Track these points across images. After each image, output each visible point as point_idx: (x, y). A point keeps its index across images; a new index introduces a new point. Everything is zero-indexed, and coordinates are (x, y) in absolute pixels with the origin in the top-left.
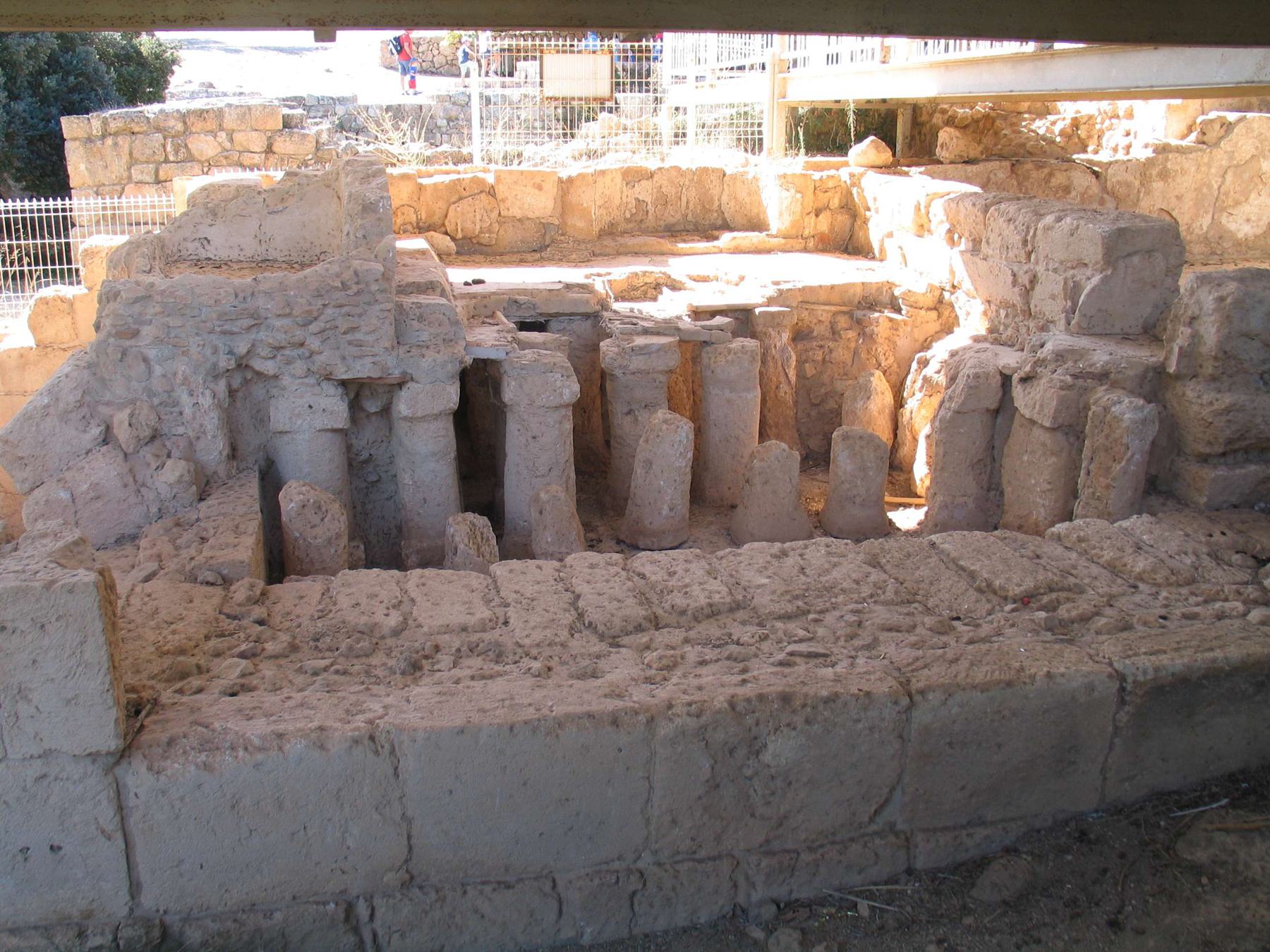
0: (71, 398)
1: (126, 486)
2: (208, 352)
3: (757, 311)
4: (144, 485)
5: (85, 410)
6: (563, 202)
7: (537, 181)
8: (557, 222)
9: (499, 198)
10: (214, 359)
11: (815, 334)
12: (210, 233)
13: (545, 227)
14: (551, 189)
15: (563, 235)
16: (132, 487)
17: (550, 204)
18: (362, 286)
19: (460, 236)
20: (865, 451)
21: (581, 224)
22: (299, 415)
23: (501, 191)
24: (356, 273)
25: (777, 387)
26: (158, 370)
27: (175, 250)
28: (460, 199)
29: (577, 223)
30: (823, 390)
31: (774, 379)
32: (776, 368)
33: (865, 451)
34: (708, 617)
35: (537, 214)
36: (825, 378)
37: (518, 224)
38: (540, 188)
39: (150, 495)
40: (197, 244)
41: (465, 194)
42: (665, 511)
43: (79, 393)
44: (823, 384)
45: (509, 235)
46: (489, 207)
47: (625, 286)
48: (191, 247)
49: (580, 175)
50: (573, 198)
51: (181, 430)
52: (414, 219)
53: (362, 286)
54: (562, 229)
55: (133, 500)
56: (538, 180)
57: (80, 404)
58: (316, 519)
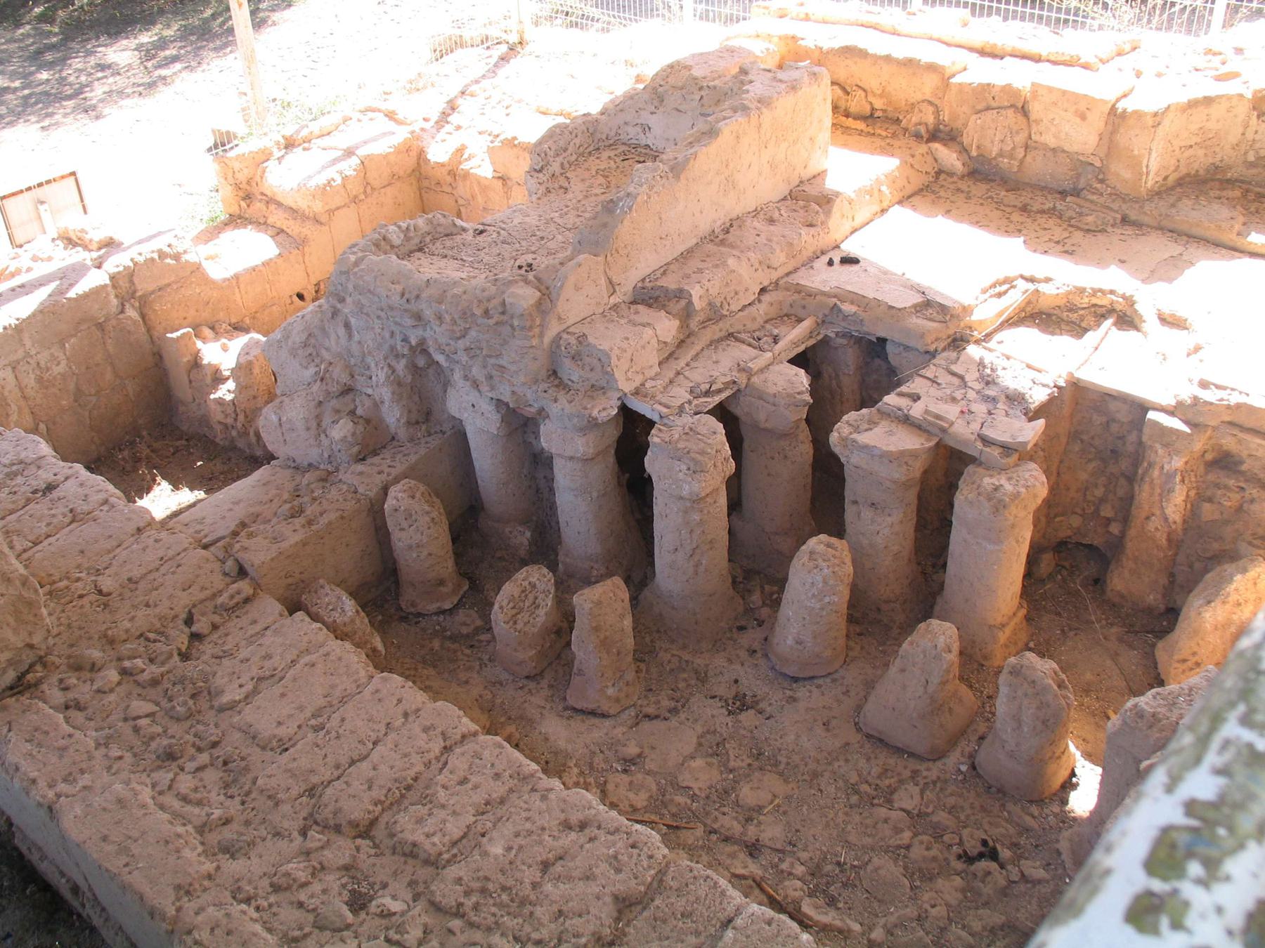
0: (298, 340)
1: (308, 429)
2: (387, 335)
3: (1152, 415)
4: (324, 432)
5: (310, 350)
6: (1111, 140)
7: (1081, 106)
8: (1098, 164)
9: (1033, 116)
10: (392, 342)
11: (1244, 467)
12: (652, 121)
13: (1080, 164)
14: (1097, 122)
15: (1102, 181)
16: (313, 432)
17: (1093, 140)
18: (505, 318)
19: (974, 153)
20: (1026, 702)
21: (1127, 174)
22: (465, 409)
23: (1036, 109)
24: (503, 303)
25: (1148, 518)
26: (356, 337)
27: (612, 134)
28: (988, 108)
29: (1121, 172)
30: (1216, 546)
31: (1146, 507)
32: (1151, 495)
33: (1026, 702)
34: (405, 855)
35: (1075, 148)
36: (1228, 531)
37: (1050, 154)
38: (1083, 117)
39: (325, 442)
40: (639, 129)
41: (994, 104)
42: (790, 641)
43: (304, 337)
44: (1220, 539)
45: (1037, 166)
46: (1015, 128)
47: (1062, 302)
48: (632, 131)
49: (1135, 112)
50: (1122, 139)
51: (370, 391)
52: (931, 120)
53: (505, 318)
54: (1101, 175)
55: (312, 441)
56: (1082, 106)
57: (305, 345)
58: (405, 524)
